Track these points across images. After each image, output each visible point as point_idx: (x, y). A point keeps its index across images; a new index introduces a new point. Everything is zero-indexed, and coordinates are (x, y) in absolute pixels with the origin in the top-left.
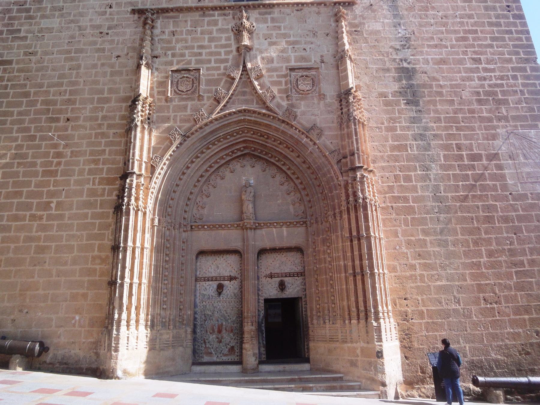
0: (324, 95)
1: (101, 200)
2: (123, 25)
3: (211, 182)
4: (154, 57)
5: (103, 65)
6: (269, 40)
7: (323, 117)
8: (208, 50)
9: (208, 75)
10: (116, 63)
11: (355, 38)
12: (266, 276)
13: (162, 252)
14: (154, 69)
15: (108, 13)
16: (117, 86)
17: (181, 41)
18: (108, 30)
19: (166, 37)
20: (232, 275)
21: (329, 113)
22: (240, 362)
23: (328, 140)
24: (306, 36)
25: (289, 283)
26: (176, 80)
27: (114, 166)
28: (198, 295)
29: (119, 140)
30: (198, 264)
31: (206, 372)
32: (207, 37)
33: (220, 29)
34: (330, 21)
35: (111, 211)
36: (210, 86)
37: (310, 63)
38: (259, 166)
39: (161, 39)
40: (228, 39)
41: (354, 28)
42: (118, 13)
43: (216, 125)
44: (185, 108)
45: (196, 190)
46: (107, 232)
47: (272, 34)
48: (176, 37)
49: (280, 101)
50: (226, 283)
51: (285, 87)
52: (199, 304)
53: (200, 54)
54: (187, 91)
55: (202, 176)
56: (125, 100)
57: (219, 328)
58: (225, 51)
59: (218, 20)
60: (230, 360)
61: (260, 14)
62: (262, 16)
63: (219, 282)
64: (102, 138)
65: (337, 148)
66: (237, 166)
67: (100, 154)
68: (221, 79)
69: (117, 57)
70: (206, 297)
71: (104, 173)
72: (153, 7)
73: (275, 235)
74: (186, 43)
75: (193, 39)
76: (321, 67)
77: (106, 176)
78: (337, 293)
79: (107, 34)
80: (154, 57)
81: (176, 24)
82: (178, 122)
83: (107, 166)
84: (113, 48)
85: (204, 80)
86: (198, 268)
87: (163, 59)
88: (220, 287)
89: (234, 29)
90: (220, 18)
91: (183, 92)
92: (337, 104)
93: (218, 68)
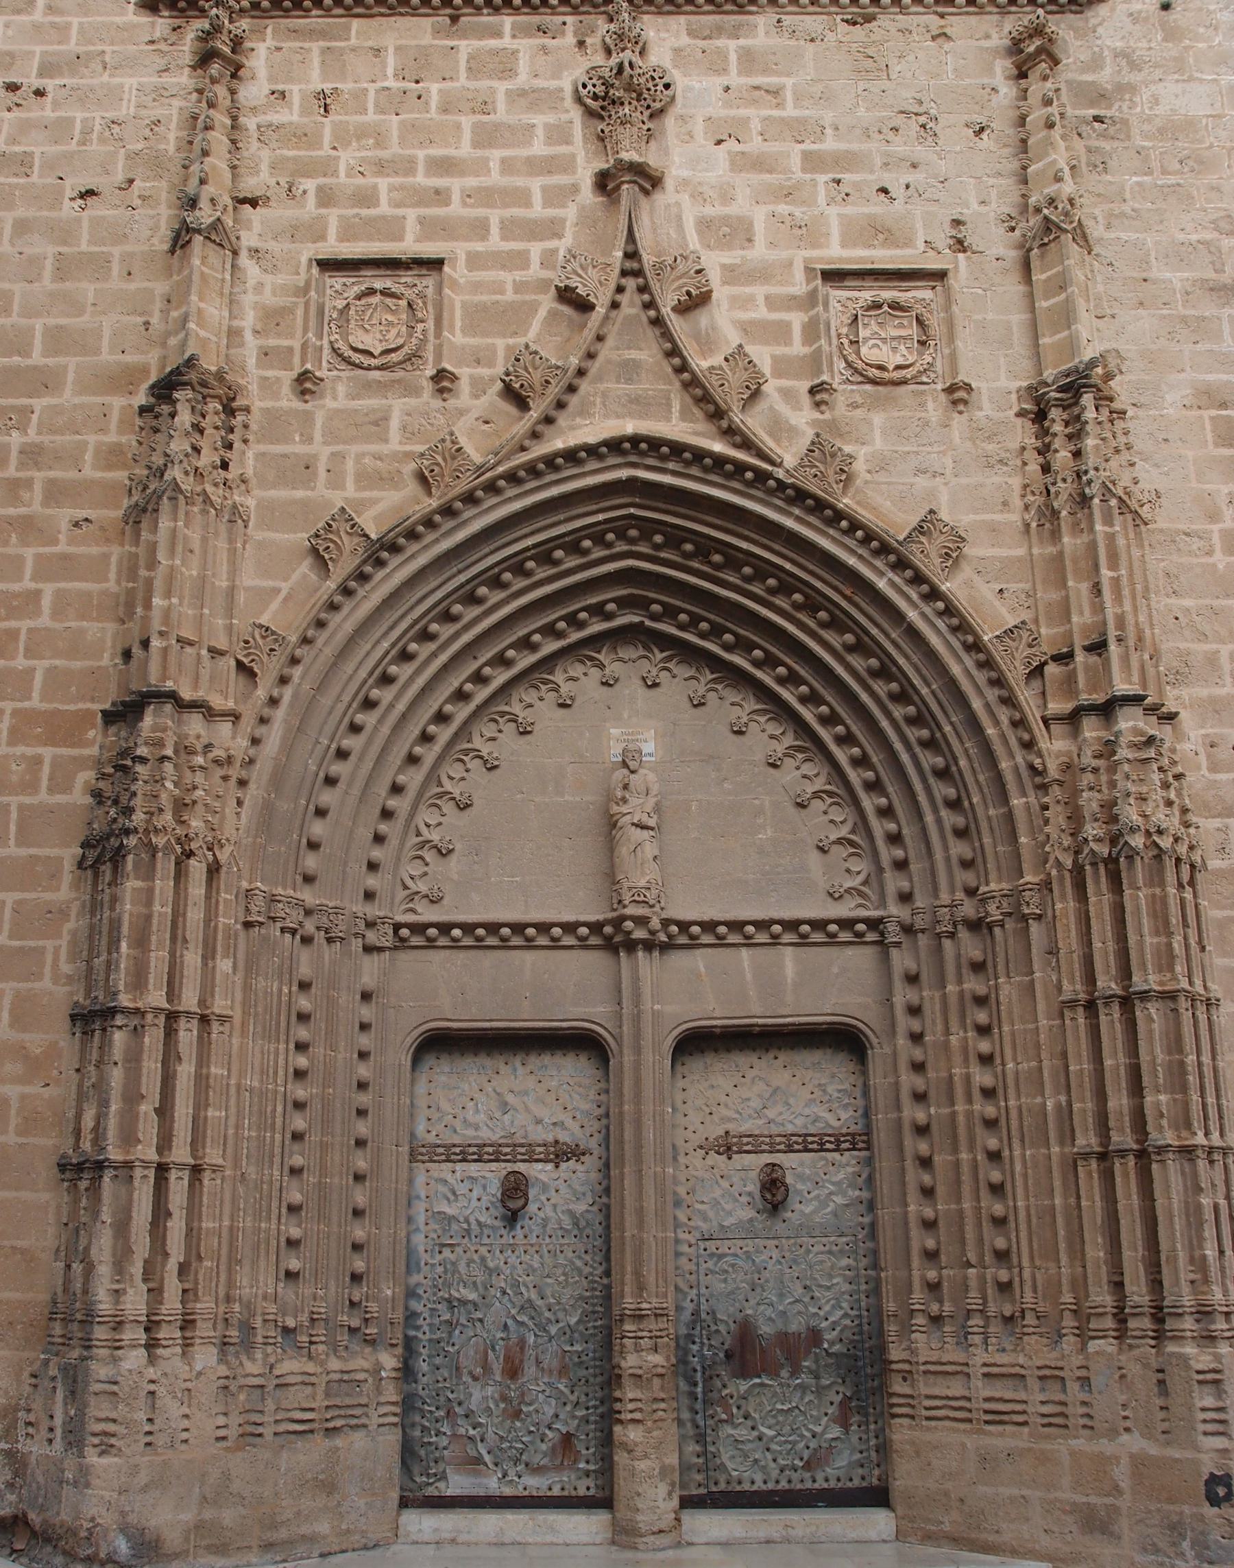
0: (968, 388)
1: (21, 808)
2: (107, 59)
3: (477, 743)
4: (244, 201)
6: (731, 145)
7: (964, 481)
8: (472, 182)
9: (477, 287)
10: (78, 220)
11: (1097, 150)
12: (706, 1148)
13: (283, 1037)
14: (244, 254)
17: (359, 139)
18: (40, 75)
20: (564, 1137)
22: (603, 1501)
23: (993, 586)
24: (891, 136)
25: (801, 1177)
26: (340, 304)
27: (77, 665)
28: (421, 1219)
29: (95, 550)
30: (421, 1088)
31: (462, 1538)
32: (467, 121)
33: (522, 93)
34: (990, 71)
36: (486, 334)
37: (908, 252)
38: (680, 683)
40: (558, 134)
41: (1092, 104)
43: (510, 500)
44: (380, 421)
45: (413, 779)
46: (49, 944)
47: (745, 121)
48: (332, 117)
49: (783, 408)
50: (539, 1172)
51: (806, 350)
52: (425, 1257)
53: (441, 196)
55: (441, 718)
56: (123, 380)
57: (507, 1358)
58: (545, 189)
59: (515, 52)
60: (556, 1492)
61: (691, 33)
63: (510, 1167)
64: (25, 543)
66: (578, 680)
67: (12, 613)
68: (533, 308)
70: (455, 1227)
71: (36, 695)
73: (749, 976)
74: (379, 145)
75: (410, 129)
76: (956, 267)
77: (45, 706)
79: (39, 93)
80: (244, 201)
83: (46, 663)
84: (69, 157)
85: (458, 305)
86: (422, 1103)
88: (515, 1193)
89: (584, 92)
90: (526, 45)
92: (1023, 434)
93: (519, 260)
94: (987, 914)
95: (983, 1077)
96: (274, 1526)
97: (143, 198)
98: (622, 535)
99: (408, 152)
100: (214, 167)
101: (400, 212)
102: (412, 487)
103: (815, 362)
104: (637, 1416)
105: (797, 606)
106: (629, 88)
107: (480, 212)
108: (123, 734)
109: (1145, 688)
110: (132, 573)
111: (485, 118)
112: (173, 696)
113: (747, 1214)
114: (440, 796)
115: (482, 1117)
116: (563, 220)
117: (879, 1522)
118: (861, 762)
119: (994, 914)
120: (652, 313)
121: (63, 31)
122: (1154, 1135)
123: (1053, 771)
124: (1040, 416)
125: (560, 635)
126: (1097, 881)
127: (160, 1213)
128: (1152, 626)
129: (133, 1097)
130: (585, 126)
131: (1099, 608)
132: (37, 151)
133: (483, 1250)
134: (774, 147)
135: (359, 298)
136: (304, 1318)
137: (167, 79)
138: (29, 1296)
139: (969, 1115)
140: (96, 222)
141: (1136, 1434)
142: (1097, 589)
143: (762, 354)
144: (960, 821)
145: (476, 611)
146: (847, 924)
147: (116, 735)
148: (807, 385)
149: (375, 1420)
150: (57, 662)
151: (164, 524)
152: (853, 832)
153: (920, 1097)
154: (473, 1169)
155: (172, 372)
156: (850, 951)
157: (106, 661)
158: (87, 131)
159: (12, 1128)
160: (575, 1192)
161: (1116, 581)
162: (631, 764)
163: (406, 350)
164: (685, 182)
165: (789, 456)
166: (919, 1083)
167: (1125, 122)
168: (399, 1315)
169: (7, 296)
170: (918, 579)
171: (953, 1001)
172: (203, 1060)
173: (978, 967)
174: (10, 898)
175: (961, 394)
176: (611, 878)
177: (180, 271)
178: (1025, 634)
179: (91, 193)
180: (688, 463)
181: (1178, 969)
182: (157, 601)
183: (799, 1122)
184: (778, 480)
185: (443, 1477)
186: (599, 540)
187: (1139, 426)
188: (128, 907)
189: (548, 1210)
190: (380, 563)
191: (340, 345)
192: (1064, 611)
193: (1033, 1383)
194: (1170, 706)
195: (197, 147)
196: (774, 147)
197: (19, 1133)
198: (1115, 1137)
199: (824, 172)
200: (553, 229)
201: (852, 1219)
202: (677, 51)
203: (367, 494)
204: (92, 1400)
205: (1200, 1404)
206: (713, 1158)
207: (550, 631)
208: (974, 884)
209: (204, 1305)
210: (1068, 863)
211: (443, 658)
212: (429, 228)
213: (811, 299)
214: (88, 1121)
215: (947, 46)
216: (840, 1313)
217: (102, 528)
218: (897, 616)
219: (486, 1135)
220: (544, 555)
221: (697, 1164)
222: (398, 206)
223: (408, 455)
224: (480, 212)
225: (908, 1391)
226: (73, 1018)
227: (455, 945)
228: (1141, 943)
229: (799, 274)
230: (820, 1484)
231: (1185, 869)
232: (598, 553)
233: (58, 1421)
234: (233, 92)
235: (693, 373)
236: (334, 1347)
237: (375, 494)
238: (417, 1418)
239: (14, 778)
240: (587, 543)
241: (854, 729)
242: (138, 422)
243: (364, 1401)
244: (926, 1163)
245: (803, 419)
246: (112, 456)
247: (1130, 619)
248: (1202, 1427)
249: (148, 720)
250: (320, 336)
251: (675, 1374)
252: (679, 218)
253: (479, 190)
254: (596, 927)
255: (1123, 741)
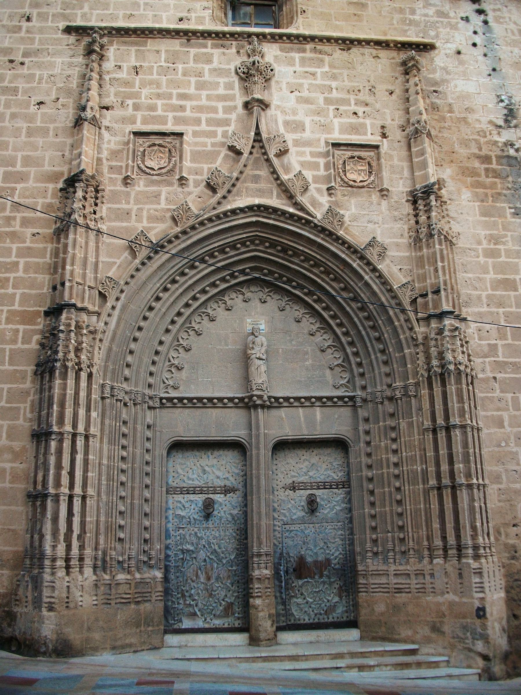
0: (388, 190)
1: (11, 350)
2: (50, 51)
3: (193, 324)
4: (104, 108)
5: (13, 116)
6: (296, 93)
8: (195, 103)
9: (196, 144)
10: (36, 114)
12: (285, 488)
13: (117, 443)
15: (24, 29)
16: (38, 153)
17: (150, 85)
19: (123, 75)
20: (228, 483)
21: (396, 220)
23: (396, 267)
24: (358, 93)
25: (322, 499)
26: (141, 149)
27: (33, 292)
28: (171, 518)
29: (41, 246)
31: (189, 645)
32: (193, 80)
33: (215, 70)
35: (30, 369)
36: (199, 162)
38: (274, 302)
39: (114, 79)
40: (229, 86)
41: (433, 86)
42: (41, 30)
43: (209, 228)
44: (157, 196)
45: (167, 339)
46: (22, 406)
47: (301, 85)
48: (140, 76)
49: (316, 195)
50: (218, 498)
51: (325, 173)
52: (172, 533)
53: (182, 108)
54: (160, 169)
55: (179, 314)
56: (54, 177)
58: (223, 107)
59: (212, 54)
60: (226, 626)
61: (281, 50)
62: (285, 54)
63: (207, 496)
64: (13, 243)
65: (409, 279)
66: (235, 300)
67: (7, 270)
68: (219, 153)
69: (38, 104)
70: (184, 520)
71: (17, 304)
72: (103, 25)
73: (302, 419)
74: (158, 87)
77: (20, 309)
78: (409, 517)
79: (22, 64)
80: (104, 108)
81: (140, 55)
82: (145, 221)
83: (21, 291)
84: (33, 88)
85: (189, 151)
86: (171, 470)
87: (117, 113)
89: (239, 71)
91: (153, 169)
92: (408, 208)
94: (396, 395)
95: (394, 459)
96: (116, 640)
97: (63, 105)
98: (252, 242)
99: (169, 91)
100: (92, 95)
101: (166, 114)
102: (169, 223)
103: (328, 179)
104: (259, 594)
105: (322, 272)
106: (257, 70)
107: (199, 115)
108: (53, 320)
109: (454, 307)
110: (57, 255)
111: (200, 79)
112: (74, 305)
113: (301, 514)
114: (179, 345)
115: (195, 476)
116: (231, 120)
117: (354, 634)
118: (346, 334)
119: (398, 395)
120: (266, 157)
121: (32, 40)
122: (458, 479)
123: (420, 337)
124: (415, 203)
125: (227, 281)
126: (437, 383)
127: (70, 513)
128: (457, 284)
129: (59, 467)
130: (239, 83)
131: (437, 277)
132: (21, 86)
133: (196, 530)
134: (313, 95)
135: (149, 147)
136: (126, 557)
137: (74, 60)
138: (16, 549)
139: (388, 473)
140: (44, 115)
141: (451, 594)
142: (436, 270)
143: (309, 175)
144: (385, 358)
145: (194, 272)
146: (341, 398)
147: (51, 320)
148: (327, 187)
149: (154, 598)
150: (25, 291)
151: (71, 236)
152: (343, 362)
153: (370, 467)
154: (192, 497)
155: (74, 175)
156: (342, 409)
157: (45, 291)
158: (41, 79)
159: (7, 480)
160: (233, 506)
161: (443, 267)
162: (256, 334)
163: (168, 168)
164: (278, 107)
165: (319, 214)
166: (369, 461)
167: (445, 93)
168: (162, 556)
169: (7, 143)
170: (369, 263)
171: (382, 428)
172: (86, 453)
173: (392, 415)
174: (6, 387)
175: (385, 193)
176: (247, 379)
177: (78, 134)
178: (410, 286)
179: (42, 103)
180: (279, 216)
181: (467, 416)
182: (68, 267)
183: (322, 477)
184: (315, 224)
185: (181, 621)
186: (244, 244)
187: (452, 209)
188: (57, 392)
189: (222, 513)
190: (156, 252)
191: (141, 165)
192: (423, 278)
193: (413, 577)
194: (464, 315)
195: (85, 87)
196: (313, 95)
197: (10, 483)
198: (444, 481)
199: (332, 105)
200: (226, 122)
201: (343, 516)
202: (276, 57)
203: (151, 225)
204: (45, 590)
205: (474, 581)
206: (288, 492)
207: (223, 280)
208: (390, 383)
209: (88, 552)
210: (426, 375)
211: (181, 290)
212: (177, 120)
213: (327, 154)
214: (40, 478)
215: (379, 61)
216: (338, 553)
217: (44, 237)
218: (361, 278)
219: (197, 483)
220: (222, 250)
221: (282, 494)
222: (165, 111)
223: (169, 210)
224: (199, 115)
225: (365, 582)
226: (33, 436)
227: (185, 407)
228: (453, 406)
229: (323, 143)
230: (331, 620)
231: (469, 378)
232: (243, 250)
233: (30, 598)
234: (100, 66)
235: (282, 181)
236: (138, 570)
237: (155, 225)
238: (170, 598)
239: (8, 338)
240: (239, 246)
241: (344, 321)
242: (60, 194)
243: (150, 590)
244: (372, 493)
245: (324, 200)
246: (48, 209)
247: (448, 282)
248: (475, 590)
249: (64, 316)
250: (133, 162)
251: (274, 578)
252: (276, 121)
253: (198, 106)
254: (241, 399)
255: (446, 328)
